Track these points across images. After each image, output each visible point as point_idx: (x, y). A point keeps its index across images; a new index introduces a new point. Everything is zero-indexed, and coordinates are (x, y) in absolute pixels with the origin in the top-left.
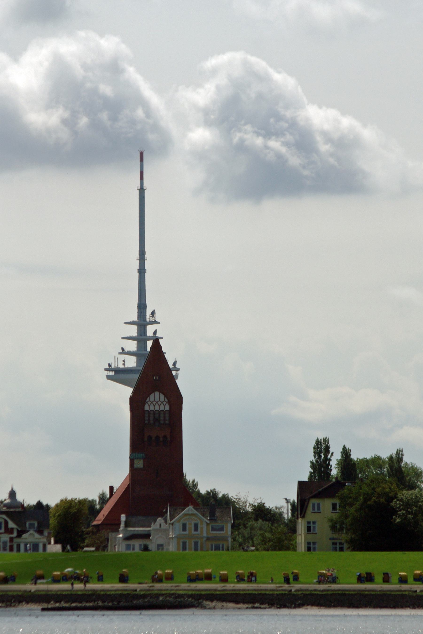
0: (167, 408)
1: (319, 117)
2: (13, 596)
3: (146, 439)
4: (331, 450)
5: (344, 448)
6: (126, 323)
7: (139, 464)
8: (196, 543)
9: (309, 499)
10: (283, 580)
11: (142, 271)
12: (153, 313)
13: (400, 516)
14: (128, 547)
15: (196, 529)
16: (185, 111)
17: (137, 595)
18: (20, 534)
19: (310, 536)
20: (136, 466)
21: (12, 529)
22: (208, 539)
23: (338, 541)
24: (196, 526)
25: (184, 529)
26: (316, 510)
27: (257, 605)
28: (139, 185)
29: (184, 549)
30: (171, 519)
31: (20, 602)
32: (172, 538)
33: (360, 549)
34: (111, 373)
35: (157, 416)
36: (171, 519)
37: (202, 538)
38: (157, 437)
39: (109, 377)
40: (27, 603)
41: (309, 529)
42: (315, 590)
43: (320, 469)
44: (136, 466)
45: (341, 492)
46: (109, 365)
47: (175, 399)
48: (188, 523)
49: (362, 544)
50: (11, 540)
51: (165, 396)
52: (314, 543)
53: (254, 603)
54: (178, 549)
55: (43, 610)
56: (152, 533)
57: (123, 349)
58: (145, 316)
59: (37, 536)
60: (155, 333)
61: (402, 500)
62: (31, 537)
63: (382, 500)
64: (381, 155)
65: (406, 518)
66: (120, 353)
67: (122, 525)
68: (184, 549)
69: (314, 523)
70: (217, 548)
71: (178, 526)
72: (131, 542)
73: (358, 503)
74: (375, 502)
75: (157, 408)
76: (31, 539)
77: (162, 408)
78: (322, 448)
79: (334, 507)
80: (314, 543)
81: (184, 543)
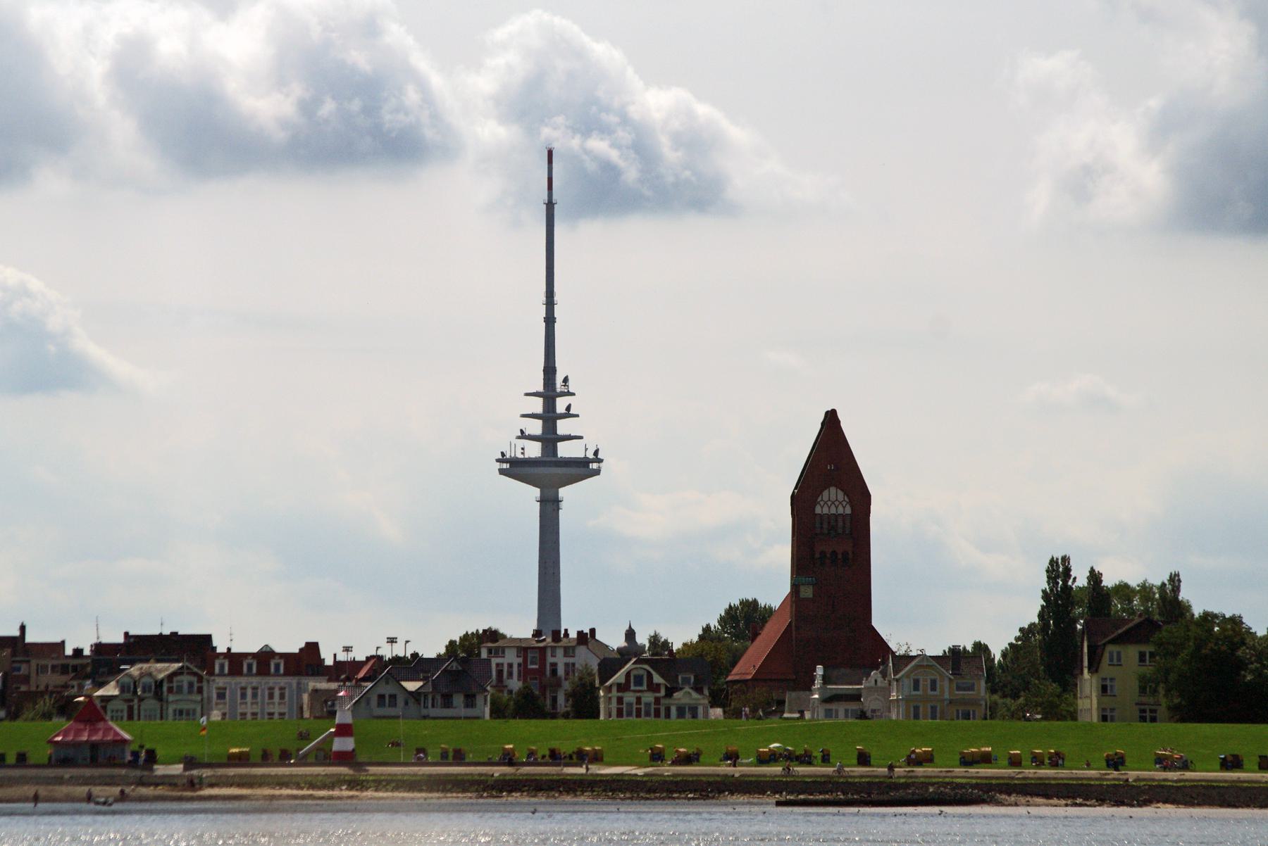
0: (848, 511)
1: (656, 103)
2: (709, 783)
3: (817, 556)
4: (1073, 574)
5: (1092, 571)
6: (527, 394)
7: (807, 592)
8: (934, 709)
9: (1104, 645)
10: (1104, 764)
11: (550, 320)
12: (566, 380)
13: (1252, 671)
14: (828, 714)
15: (933, 689)
16: (469, 92)
17: (895, 784)
18: (670, 693)
19: (1106, 699)
20: (802, 595)
21: (658, 685)
22: (951, 702)
23: (1147, 707)
24: (934, 682)
25: (916, 688)
26: (1115, 662)
27: (1079, 801)
28: (544, 196)
29: (916, 717)
30: (896, 673)
31: (721, 792)
32: (897, 700)
33: (1183, 720)
34: (505, 466)
35: (833, 523)
36: (896, 673)
37: (943, 701)
38: (834, 553)
39: (502, 472)
40: (732, 793)
41: (1104, 689)
42: (1165, 780)
43: (1056, 600)
44: (802, 595)
45: (1157, 635)
46: (503, 454)
47: (860, 497)
48: (921, 678)
49: (1192, 711)
50: (657, 700)
51: (846, 493)
52: (1112, 710)
53: (1074, 798)
54: (907, 716)
55: (779, 804)
56: (864, 693)
57: (522, 431)
58: (554, 384)
59: (695, 695)
60: (568, 408)
61: (1253, 648)
62: (685, 696)
63: (1224, 648)
64: (749, 156)
65: (1260, 675)
66: (518, 438)
67: (818, 683)
68: (916, 717)
69: (1112, 679)
70: (967, 716)
71: (908, 683)
72: (834, 706)
73: (1186, 652)
74: (1212, 649)
75: (833, 511)
76: (686, 701)
77: (841, 510)
78: (1059, 570)
79: (1142, 657)
80: (1112, 710)
81: (916, 709)
